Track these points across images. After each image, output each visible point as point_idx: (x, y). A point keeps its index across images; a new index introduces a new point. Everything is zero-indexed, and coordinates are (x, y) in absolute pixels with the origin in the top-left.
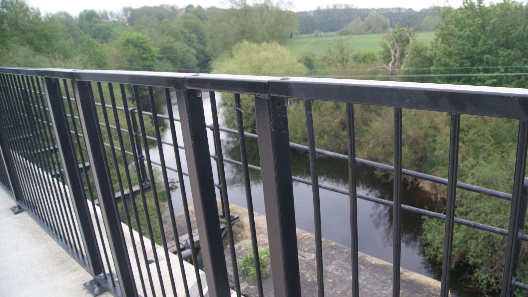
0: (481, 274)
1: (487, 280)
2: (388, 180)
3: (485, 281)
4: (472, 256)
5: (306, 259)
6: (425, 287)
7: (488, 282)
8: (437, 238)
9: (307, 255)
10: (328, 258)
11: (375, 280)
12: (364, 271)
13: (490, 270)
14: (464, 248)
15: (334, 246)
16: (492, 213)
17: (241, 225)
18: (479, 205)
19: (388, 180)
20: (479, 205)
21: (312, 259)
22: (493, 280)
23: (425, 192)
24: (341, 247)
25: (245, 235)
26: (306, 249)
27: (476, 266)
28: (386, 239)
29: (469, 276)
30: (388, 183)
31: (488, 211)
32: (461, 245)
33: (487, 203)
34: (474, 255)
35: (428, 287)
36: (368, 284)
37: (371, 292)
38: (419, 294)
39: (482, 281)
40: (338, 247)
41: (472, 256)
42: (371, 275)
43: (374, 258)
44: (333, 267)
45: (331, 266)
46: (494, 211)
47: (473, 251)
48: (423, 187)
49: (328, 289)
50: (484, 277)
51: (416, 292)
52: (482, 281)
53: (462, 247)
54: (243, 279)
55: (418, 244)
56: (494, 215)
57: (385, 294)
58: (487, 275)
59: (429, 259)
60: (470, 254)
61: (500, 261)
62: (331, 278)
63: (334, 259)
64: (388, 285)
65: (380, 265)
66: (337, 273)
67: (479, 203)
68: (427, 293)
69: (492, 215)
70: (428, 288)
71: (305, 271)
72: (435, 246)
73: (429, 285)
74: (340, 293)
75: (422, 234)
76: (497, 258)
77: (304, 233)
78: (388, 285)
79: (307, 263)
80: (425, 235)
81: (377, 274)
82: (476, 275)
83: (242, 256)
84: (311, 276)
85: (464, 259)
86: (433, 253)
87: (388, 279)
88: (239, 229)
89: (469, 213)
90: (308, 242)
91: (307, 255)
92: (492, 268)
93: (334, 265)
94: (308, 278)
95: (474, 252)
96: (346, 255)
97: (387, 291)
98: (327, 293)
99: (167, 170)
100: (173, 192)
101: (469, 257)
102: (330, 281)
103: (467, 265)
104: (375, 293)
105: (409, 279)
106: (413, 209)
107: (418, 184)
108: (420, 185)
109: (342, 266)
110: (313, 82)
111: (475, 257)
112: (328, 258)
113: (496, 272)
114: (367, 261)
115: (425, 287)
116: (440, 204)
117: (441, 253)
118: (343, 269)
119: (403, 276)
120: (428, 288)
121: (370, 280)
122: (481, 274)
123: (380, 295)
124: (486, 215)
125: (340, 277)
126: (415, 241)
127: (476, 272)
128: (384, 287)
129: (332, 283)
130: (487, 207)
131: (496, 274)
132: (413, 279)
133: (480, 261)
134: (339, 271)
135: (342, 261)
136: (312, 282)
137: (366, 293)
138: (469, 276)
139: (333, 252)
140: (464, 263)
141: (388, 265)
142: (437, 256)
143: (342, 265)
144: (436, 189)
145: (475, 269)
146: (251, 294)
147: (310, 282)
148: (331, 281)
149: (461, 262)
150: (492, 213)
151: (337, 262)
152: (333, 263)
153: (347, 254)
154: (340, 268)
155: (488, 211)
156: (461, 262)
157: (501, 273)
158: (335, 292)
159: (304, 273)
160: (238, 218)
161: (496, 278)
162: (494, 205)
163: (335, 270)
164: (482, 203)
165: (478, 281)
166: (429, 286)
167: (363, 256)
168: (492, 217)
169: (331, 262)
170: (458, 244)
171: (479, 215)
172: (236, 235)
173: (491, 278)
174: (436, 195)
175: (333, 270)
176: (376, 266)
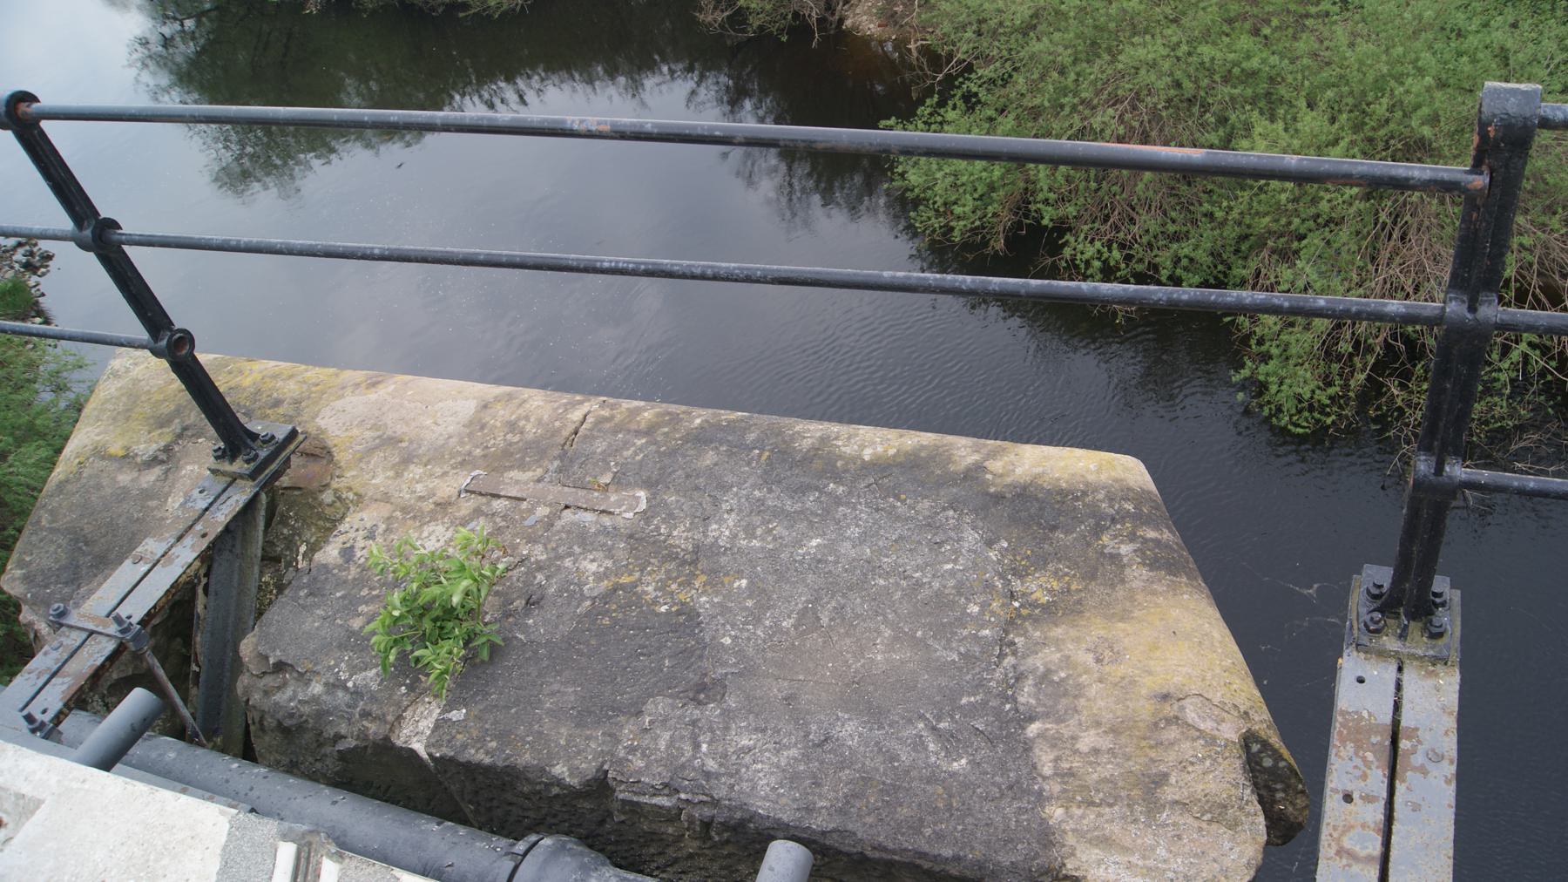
0: (1080, 247)
1: (1099, 259)
2: (744, 31)
3: (1097, 264)
4: (1046, 202)
5: (620, 522)
6: (1077, 499)
7: (1105, 262)
8: (939, 175)
9: (619, 504)
10: (697, 488)
11: (901, 530)
12: (848, 504)
13: (1103, 228)
14: (1022, 185)
15: (701, 427)
16: (1075, 62)
17: (318, 451)
18: (1036, 47)
19: (744, 31)
20: (1036, 47)
21: (644, 512)
22: (1116, 254)
23: (866, 41)
24: (731, 426)
25: (350, 489)
26: (606, 479)
27: (1062, 227)
28: (788, 214)
29: (1049, 261)
30: (750, 39)
31: (1065, 57)
32: (1010, 178)
33: (1057, 36)
34: (1052, 196)
35: (1085, 493)
36: (881, 552)
37: (904, 583)
38: (1067, 533)
39: (1088, 263)
40: (718, 427)
41: (1046, 202)
42: (877, 510)
43: (865, 432)
44: (731, 520)
45: (721, 521)
46: (1083, 56)
47: (1046, 188)
48: (856, 28)
49: (745, 623)
50: (1090, 251)
51: (1054, 528)
52: (1088, 263)
53: (1013, 183)
54: (411, 688)
55: (882, 201)
56: (1085, 65)
57: (952, 573)
58: (1098, 244)
59: (933, 242)
60: (1041, 196)
61: (1124, 195)
62: (740, 574)
63: (725, 488)
64: (952, 534)
65: (894, 456)
66: (755, 543)
67: (1034, 41)
68: (1092, 521)
69: (1078, 69)
70: (1088, 499)
71: (637, 575)
72: (940, 201)
73: (1087, 484)
74: (796, 627)
75: (893, 173)
76: (1115, 189)
77: (573, 405)
78: (952, 534)
79: (631, 536)
80: (902, 175)
81: (897, 497)
82: (1067, 252)
83: (371, 589)
84: (662, 587)
85: (1026, 216)
86: (936, 223)
87: (944, 509)
88: (315, 467)
89: (1010, 76)
90: (600, 446)
91: (619, 504)
92: (1106, 219)
93: (730, 511)
94: (655, 602)
95: (1050, 190)
96: (760, 456)
97: (955, 561)
98: (749, 639)
99: (53, 130)
100: (44, 274)
101: (1040, 206)
102: (739, 587)
103: (1037, 229)
104: (919, 584)
105: (1013, 486)
106: (1023, 286)
107: (841, 21)
108: (848, 23)
109: (759, 507)
110: (180, 237)
111: (1055, 205)
112: (697, 488)
113: (1118, 230)
114: (840, 457)
115: (1077, 499)
116: (922, 69)
117: (959, 218)
118: (769, 522)
119: (989, 477)
120: (1088, 499)
121: (882, 532)
122: (1080, 247)
123: (936, 585)
124: (1062, 72)
125: (772, 555)
126: (870, 195)
127: (1066, 244)
128: (940, 544)
129: (752, 591)
130: (1060, 49)
131: (1121, 235)
132: (1028, 479)
133: (1071, 210)
134: (759, 532)
135: (754, 486)
136: (679, 613)
137: (887, 591)
138: (1049, 261)
139: (709, 458)
140: (1028, 226)
141: (923, 447)
142: (952, 229)
143: (761, 501)
144: (896, 23)
145: (1062, 234)
146: (465, 746)
147: (668, 613)
148: (744, 582)
149: (1019, 225)
150: (1075, 62)
151: (736, 494)
152: (725, 506)
153: (762, 450)
154: (757, 520)
155: (1065, 57)
156: (1018, 225)
157: (1132, 227)
158: (777, 628)
159: (634, 585)
160: (293, 434)
161: (1122, 246)
162: (1078, 37)
163: (742, 535)
164: (1045, 39)
165: (1077, 267)
166: (1089, 489)
167: (824, 440)
168: (1078, 74)
169: (716, 503)
170: (1002, 178)
171: (1042, 77)
172: (315, 499)
173: (1110, 250)
174: (900, 44)
175: (734, 536)
176: (880, 467)
